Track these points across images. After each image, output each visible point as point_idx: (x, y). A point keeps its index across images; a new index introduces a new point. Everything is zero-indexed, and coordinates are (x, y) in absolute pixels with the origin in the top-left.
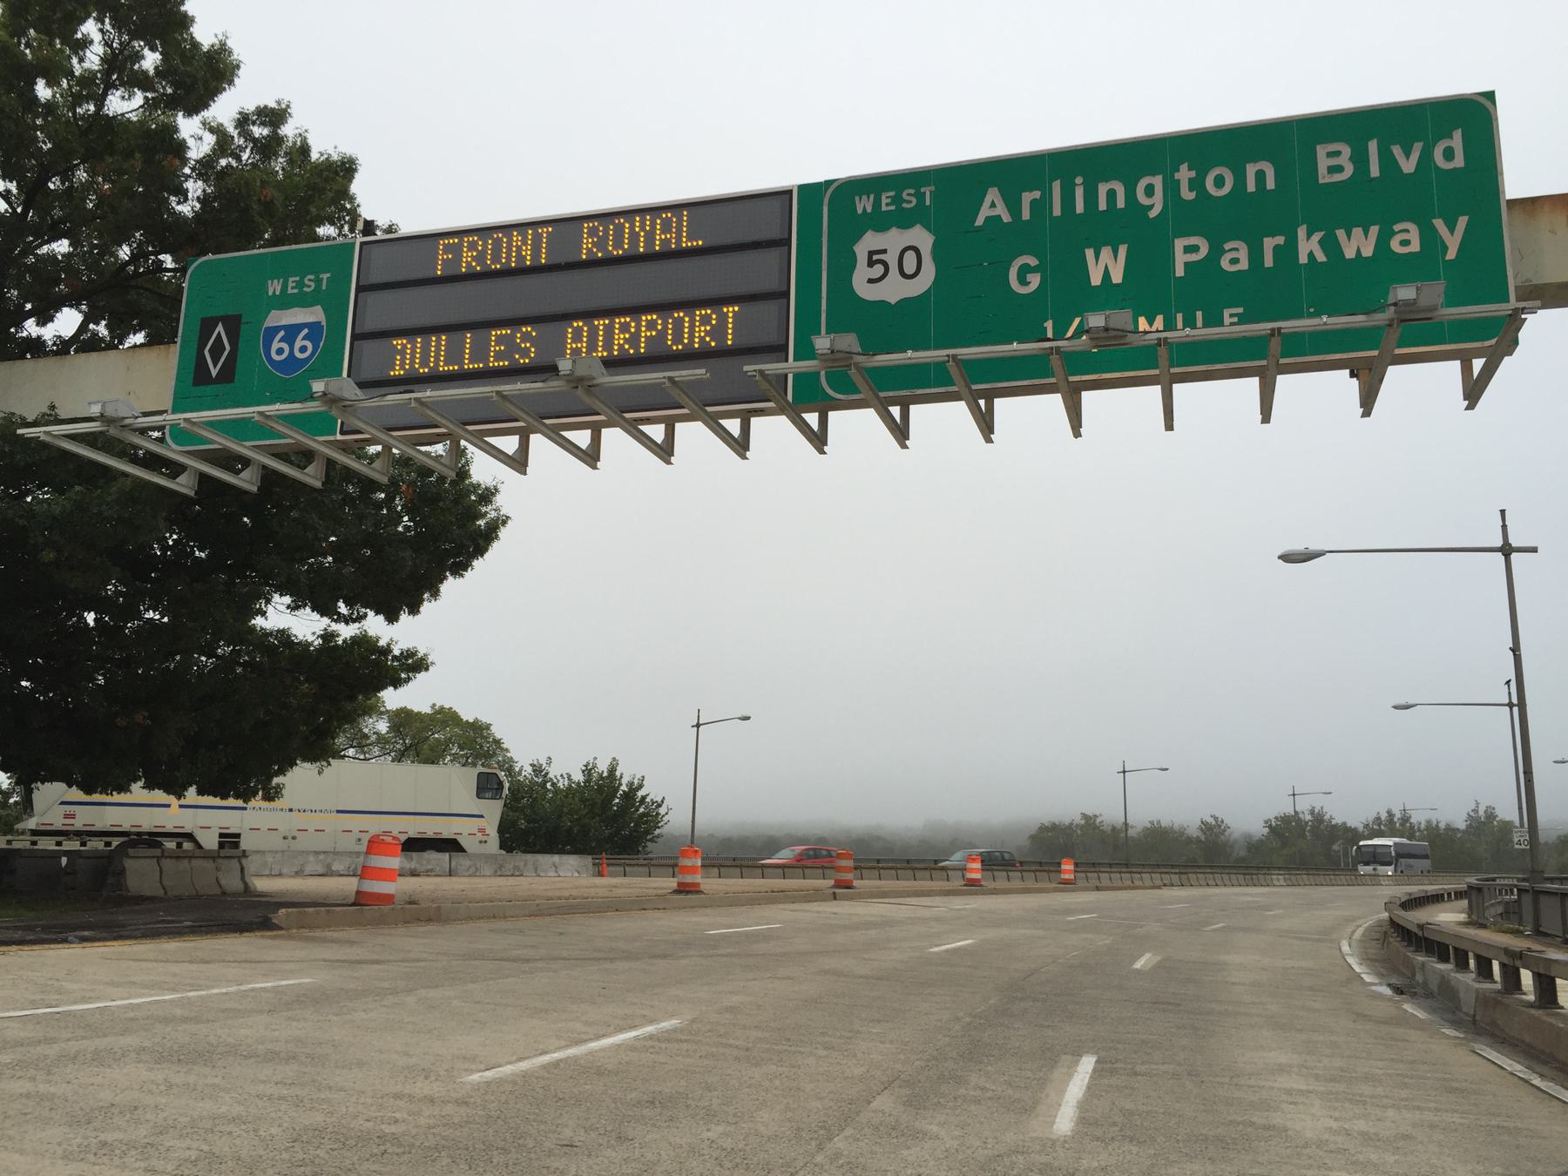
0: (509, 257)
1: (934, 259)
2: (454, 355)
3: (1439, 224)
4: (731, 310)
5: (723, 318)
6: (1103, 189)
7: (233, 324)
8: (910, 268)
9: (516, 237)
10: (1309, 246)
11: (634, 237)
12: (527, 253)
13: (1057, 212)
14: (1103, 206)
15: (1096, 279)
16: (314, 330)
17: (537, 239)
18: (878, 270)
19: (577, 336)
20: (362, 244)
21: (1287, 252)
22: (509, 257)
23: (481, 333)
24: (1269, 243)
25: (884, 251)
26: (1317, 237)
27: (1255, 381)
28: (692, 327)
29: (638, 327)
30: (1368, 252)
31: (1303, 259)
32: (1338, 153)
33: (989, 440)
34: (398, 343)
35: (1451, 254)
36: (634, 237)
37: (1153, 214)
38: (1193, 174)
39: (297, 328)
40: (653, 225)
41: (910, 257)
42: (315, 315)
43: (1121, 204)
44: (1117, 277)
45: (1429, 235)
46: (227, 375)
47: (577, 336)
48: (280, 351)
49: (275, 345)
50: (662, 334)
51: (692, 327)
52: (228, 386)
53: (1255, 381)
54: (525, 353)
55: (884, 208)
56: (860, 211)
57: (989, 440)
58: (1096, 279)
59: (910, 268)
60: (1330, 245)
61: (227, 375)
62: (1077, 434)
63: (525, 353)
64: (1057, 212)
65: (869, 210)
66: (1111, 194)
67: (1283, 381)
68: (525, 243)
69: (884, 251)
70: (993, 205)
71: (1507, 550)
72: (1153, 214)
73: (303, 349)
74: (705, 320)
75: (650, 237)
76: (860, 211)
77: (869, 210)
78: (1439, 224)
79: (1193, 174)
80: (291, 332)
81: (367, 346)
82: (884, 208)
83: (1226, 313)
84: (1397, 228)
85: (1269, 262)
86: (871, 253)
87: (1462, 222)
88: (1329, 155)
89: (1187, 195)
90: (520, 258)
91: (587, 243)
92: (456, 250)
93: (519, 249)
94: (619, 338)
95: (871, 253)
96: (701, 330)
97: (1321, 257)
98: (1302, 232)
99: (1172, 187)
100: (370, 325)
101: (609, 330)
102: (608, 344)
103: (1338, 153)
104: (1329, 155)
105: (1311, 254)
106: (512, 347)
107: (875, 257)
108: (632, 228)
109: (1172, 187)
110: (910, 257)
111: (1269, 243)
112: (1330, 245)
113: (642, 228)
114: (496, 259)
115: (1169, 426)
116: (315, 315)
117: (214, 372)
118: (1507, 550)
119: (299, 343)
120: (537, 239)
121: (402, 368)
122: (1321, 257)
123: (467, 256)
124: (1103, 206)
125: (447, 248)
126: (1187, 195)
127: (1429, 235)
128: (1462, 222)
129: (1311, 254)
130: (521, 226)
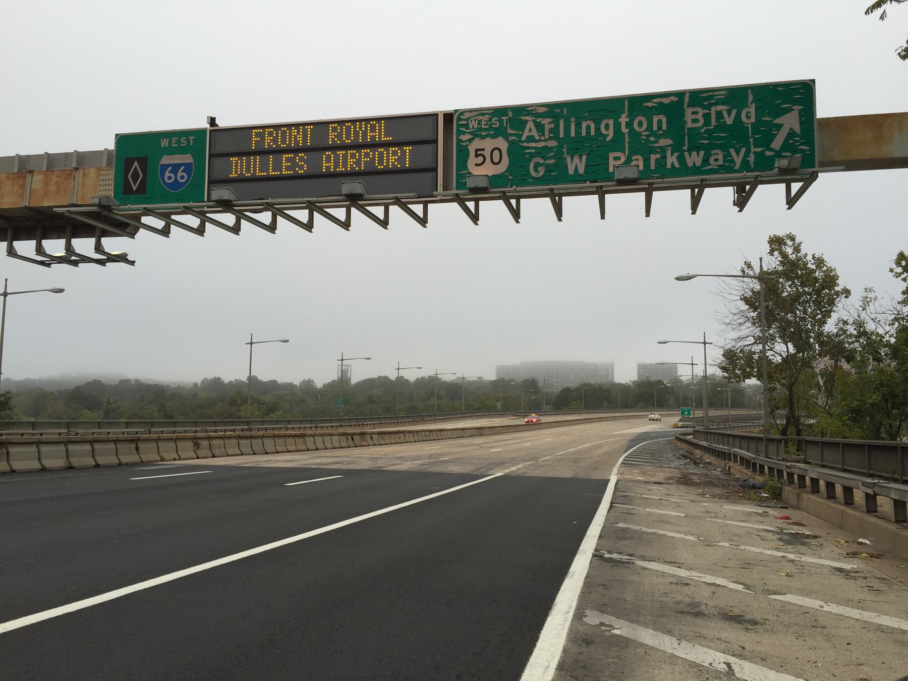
0: (290, 141)
2: (264, 167)
3: (732, 151)
4: (407, 149)
5: (404, 152)
6: (584, 125)
7: (143, 162)
9: (294, 131)
11: (356, 134)
12: (300, 138)
14: (584, 134)
15: (571, 171)
16: (188, 168)
17: (305, 131)
19: (328, 161)
20: (211, 131)
22: (290, 141)
23: (278, 156)
26: (676, 154)
27: (643, 194)
28: (388, 157)
29: (360, 156)
30: (698, 164)
31: (669, 166)
32: (697, 113)
33: (518, 222)
34: (233, 159)
36: (356, 134)
37: (608, 139)
38: (628, 120)
39: (180, 165)
40: (366, 127)
42: (188, 159)
43: (593, 133)
44: (581, 171)
45: (727, 156)
46: (142, 189)
47: (328, 161)
48: (170, 178)
49: (167, 174)
50: (373, 159)
51: (388, 157)
52: (143, 196)
53: (643, 194)
54: (301, 167)
57: (518, 222)
58: (571, 171)
61: (142, 189)
62: (560, 220)
63: (301, 167)
66: (588, 127)
67: (655, 194)
68: (298, 134)
70: (530, 130)
71: (705, 343)
72: (608, 139)
73: (182, 177)
74: (395, 153)
75: (365, 134)
78: (732, 151)
79: (628, 120)
80: (175, 168)
81: (218, 161)
84: (713, 152)
85: (653, 166)
88: (693, 113)
90: (297, 142)
91: (332, 135)
92: (261, 135)
93: (298, 134)
94: (351, 161)
96: (392, 159)
97: (677, 165)
100: (219, 149)
101: (345, 157)
102: (345, 165)
103: (697, 113)
104: (693, 113)
105: (672, 164)
106: (294, 165)
108: (355, 128)
111: (653, 157)
113: (360, 128)
114: (283, 142)
115: (603, 217)
116: (188, 159)
117: (135, 188)
118: (705, 343)
119: (180, 174)
120: (305, 131)
121: (236, 173)
122: (677, 165)
123: (268, 139)
124: (584, 134)
125: (257, 135)
127: (727, 156)
129: (672, 164)
130: (297, 125)
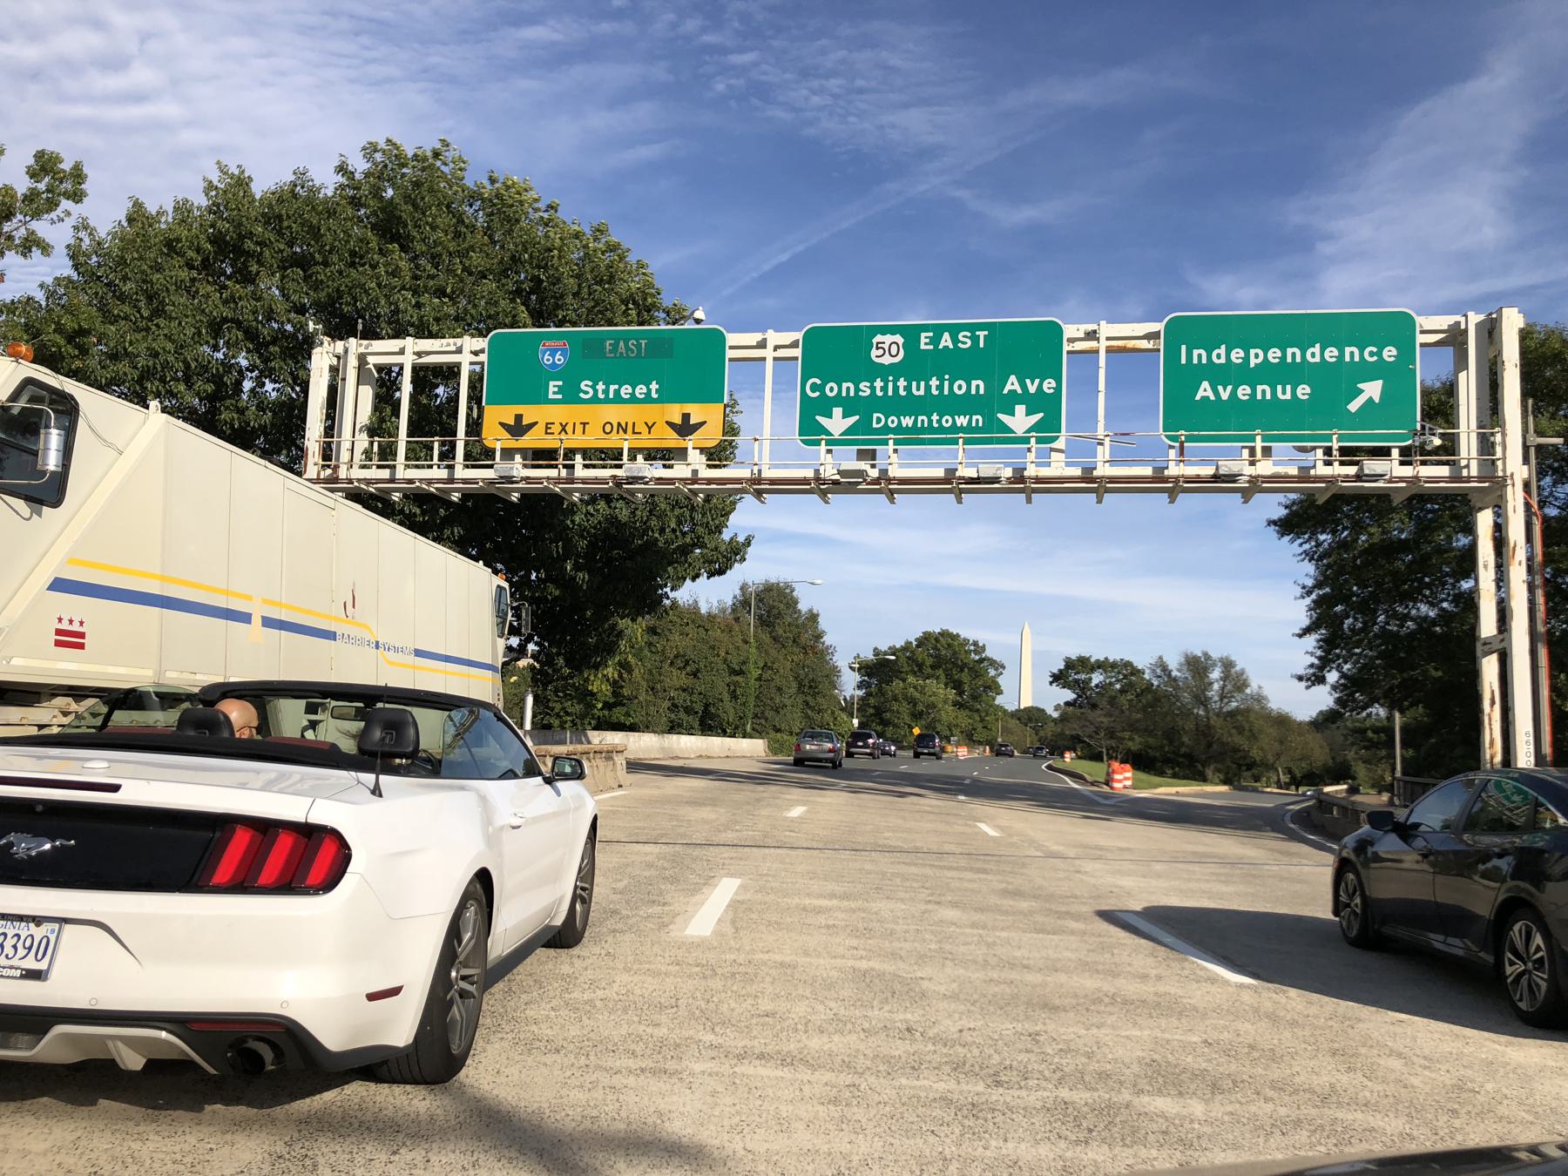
6: (1196, 352)
8: (894, 352)
13: (1183, 361)
41: (894, 348)
59: (894, 352)
64: (1183, 361)
83: (552, 383)
99: (873, 388)
110: (894, 348)
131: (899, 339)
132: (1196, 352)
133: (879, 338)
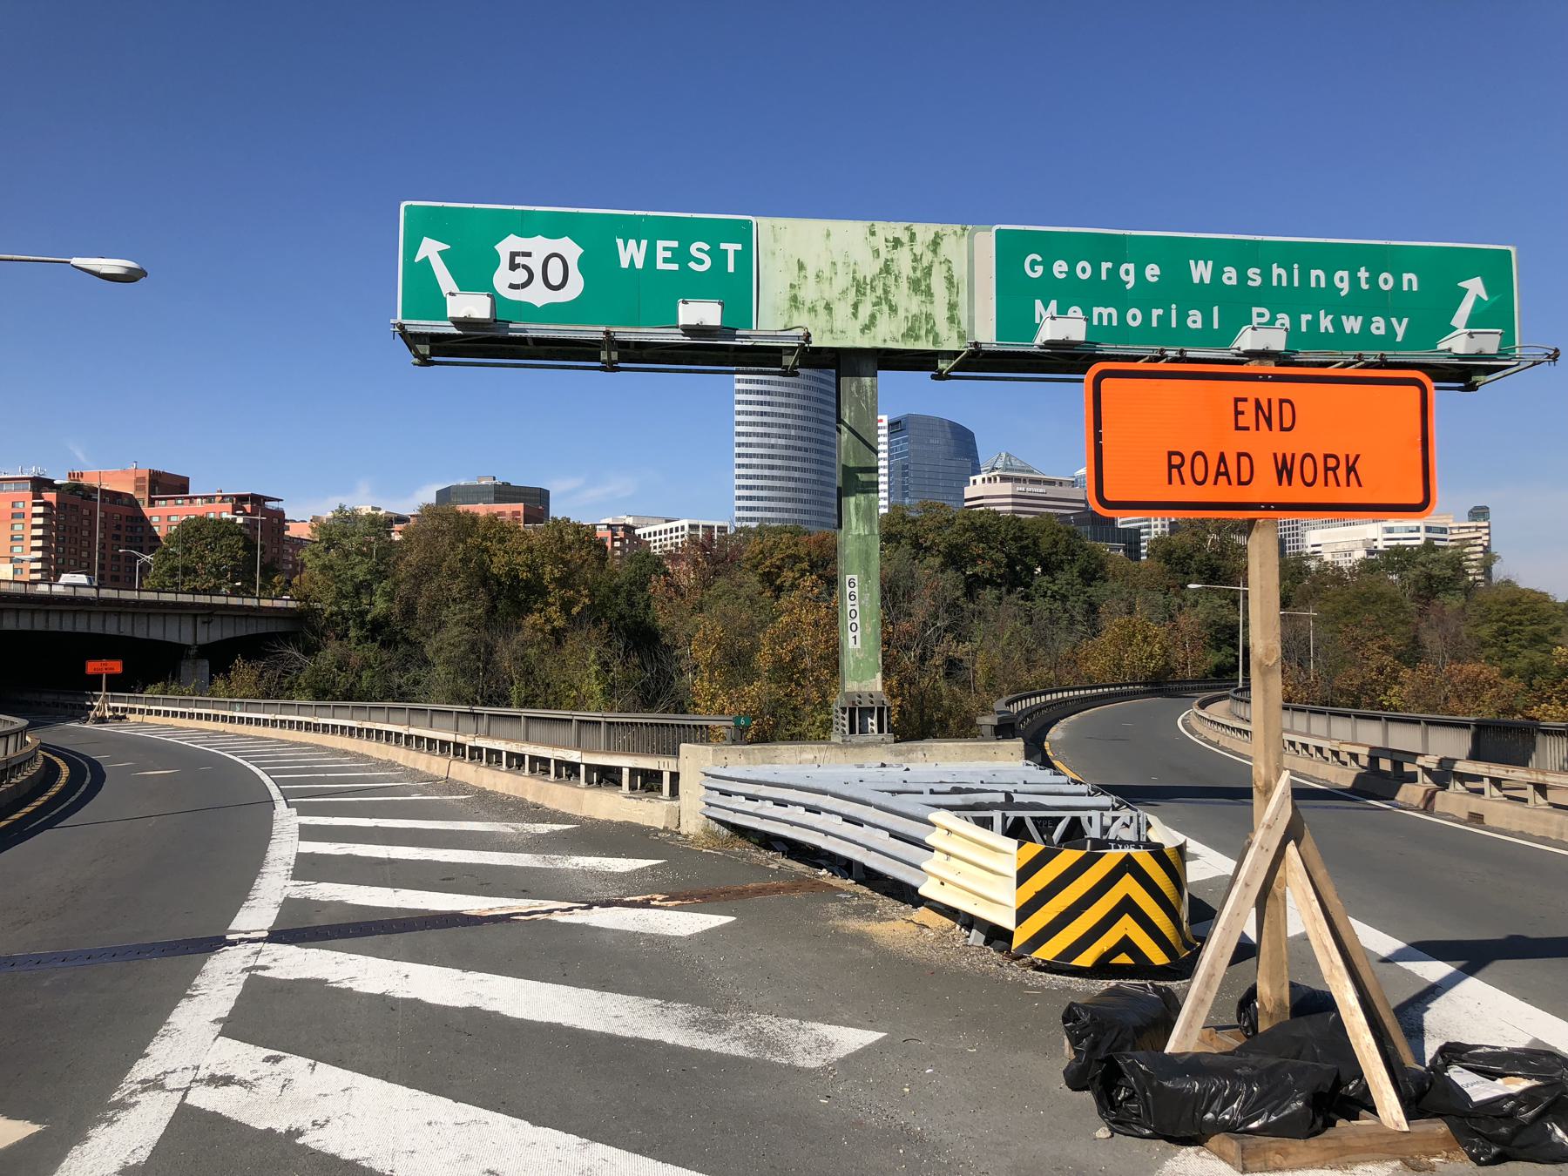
1: (472, 1013)
3: (1394, 320)
6: (1314, 273)
8: (555, 277)
10: (1325, 323)
18: (520, 276)
21: (1313, 324)
24: (1305, 318)
25: (529, 254)
35: (1399, 339)
41: (555, 264)
45: (1389, 326)
55: (660, 265)
56: (625, 264)
59: (555, 277)
60: (1337, 324)
65: (639, 265)
69: (529, 254)
76: (625, 264)
77: (639, 265)
78: (1394, 320)
82: (660, 265)
86: (513, 255)
87: (1405, 320)
89: (1365, 286)
95: (513, 255)
97: (1331, 330)
98: (1322, 313)
99: (1354, 281)
107: (518, 260)
109: (1354, 281)
110: (555, 264)
112: (1337, 324)
126: (1365, 286)
127: (1389, 326)
128: (1405, 320)
131: (571, 250)
132: (1314, 273)
133: (509, 245)
